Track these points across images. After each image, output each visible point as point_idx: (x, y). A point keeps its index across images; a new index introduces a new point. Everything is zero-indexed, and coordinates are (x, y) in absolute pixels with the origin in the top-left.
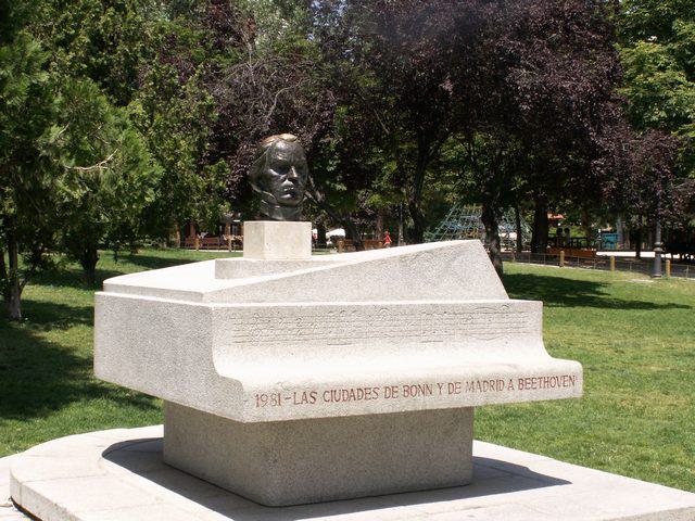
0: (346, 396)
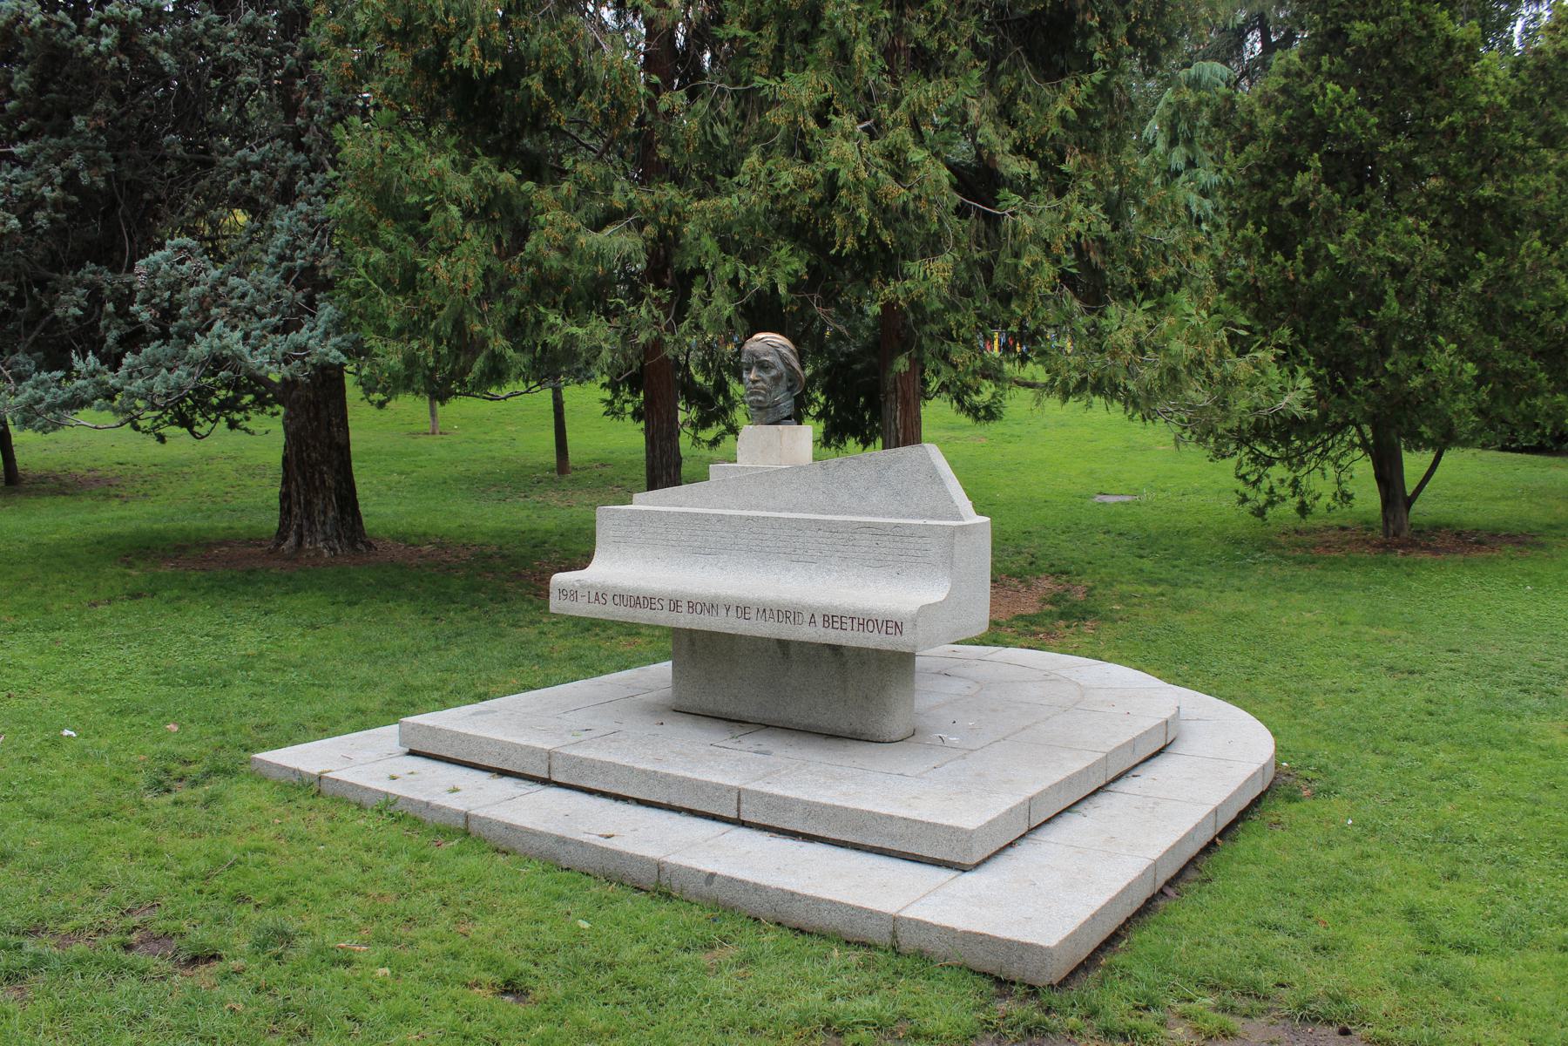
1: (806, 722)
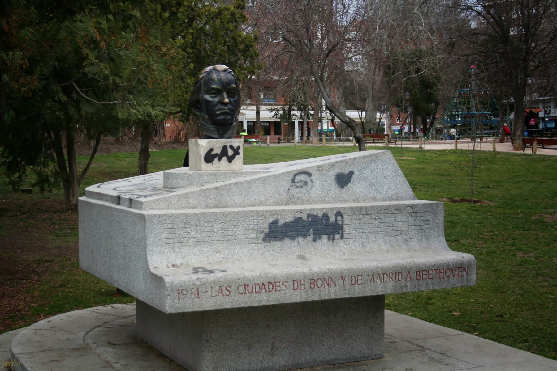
0: (258, 289)
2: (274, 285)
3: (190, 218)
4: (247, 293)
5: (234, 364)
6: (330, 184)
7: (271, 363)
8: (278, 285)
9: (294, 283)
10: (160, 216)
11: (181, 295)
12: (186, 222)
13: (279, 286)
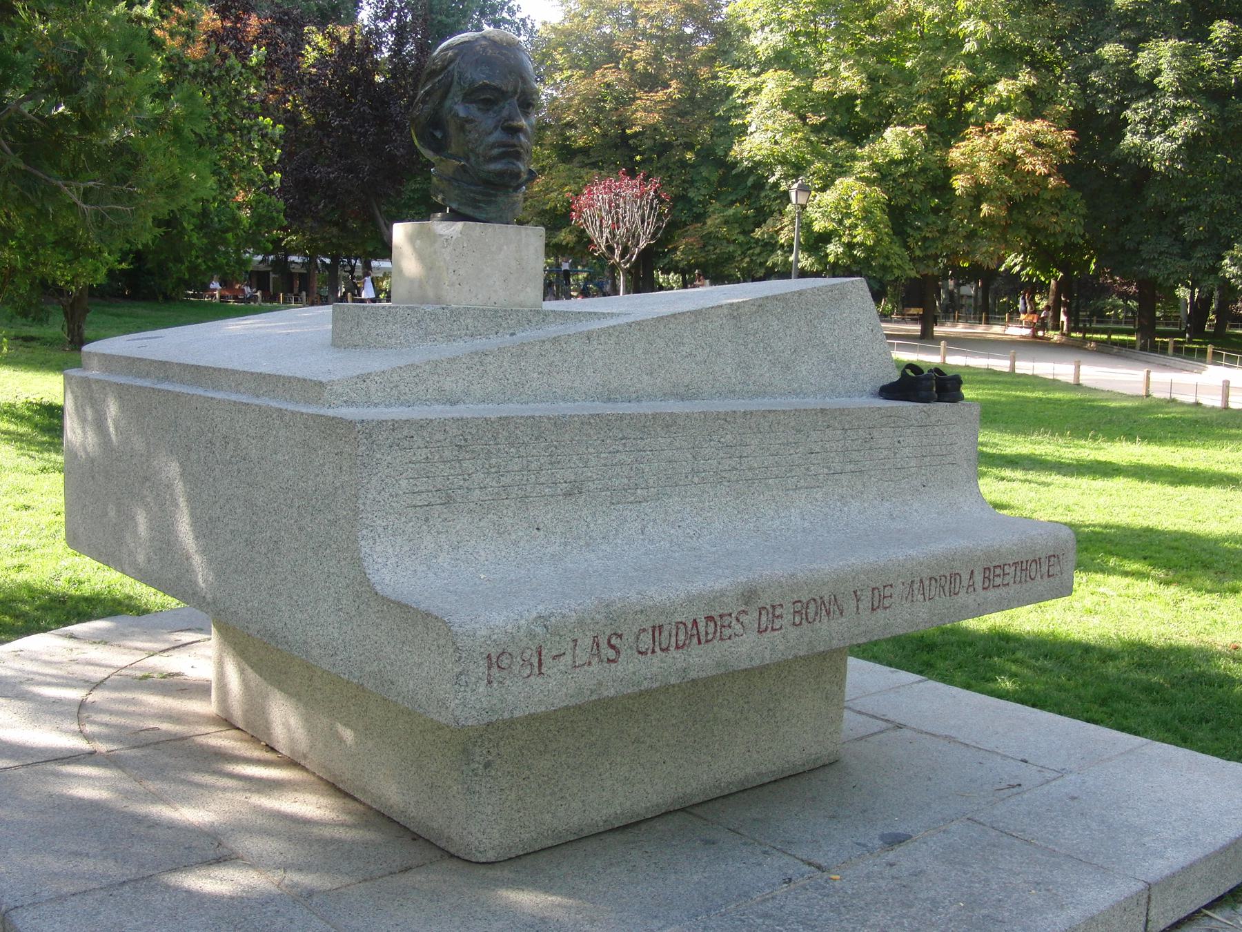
0: (682, 637)
1: (741, 775)
2: (719, 623)
3: (474, 431)
4: (657, 649)
5: (548, 816)
6: (752, 352)
7: (628, 803)
8: (726, 623)
9: (760, 614)
10: (395, 426)
11: (495, 670)
12: (463, 443)
13: (730, 626)
